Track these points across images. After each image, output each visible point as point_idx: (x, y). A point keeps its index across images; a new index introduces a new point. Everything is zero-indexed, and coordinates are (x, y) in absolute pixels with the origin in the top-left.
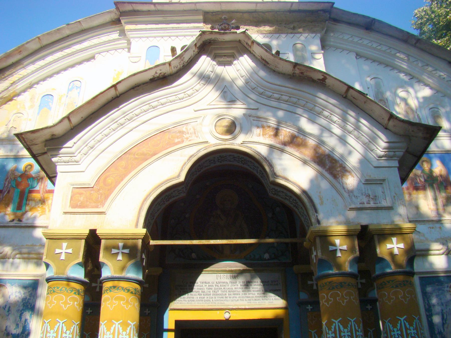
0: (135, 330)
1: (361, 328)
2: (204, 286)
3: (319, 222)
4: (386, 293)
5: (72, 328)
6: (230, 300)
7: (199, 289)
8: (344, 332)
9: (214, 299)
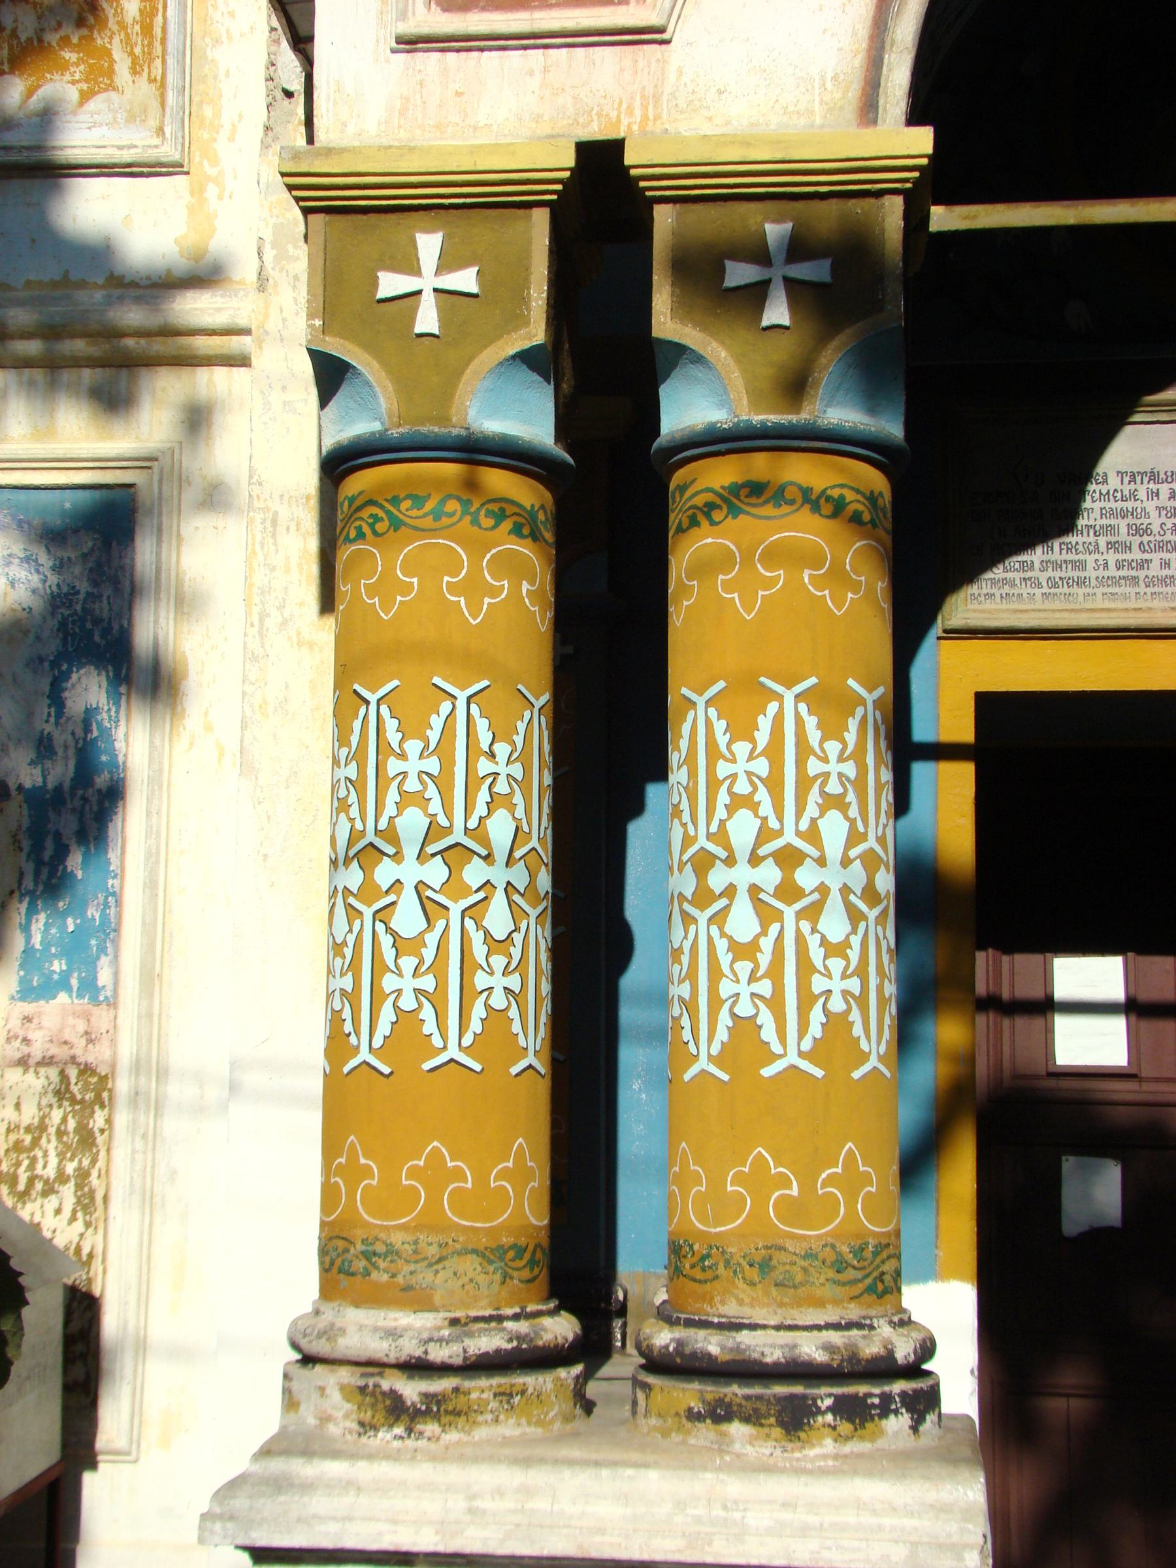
0: (882, 729)
2: (1142, 494)
5: (521, 727)
7: (1112, 513)
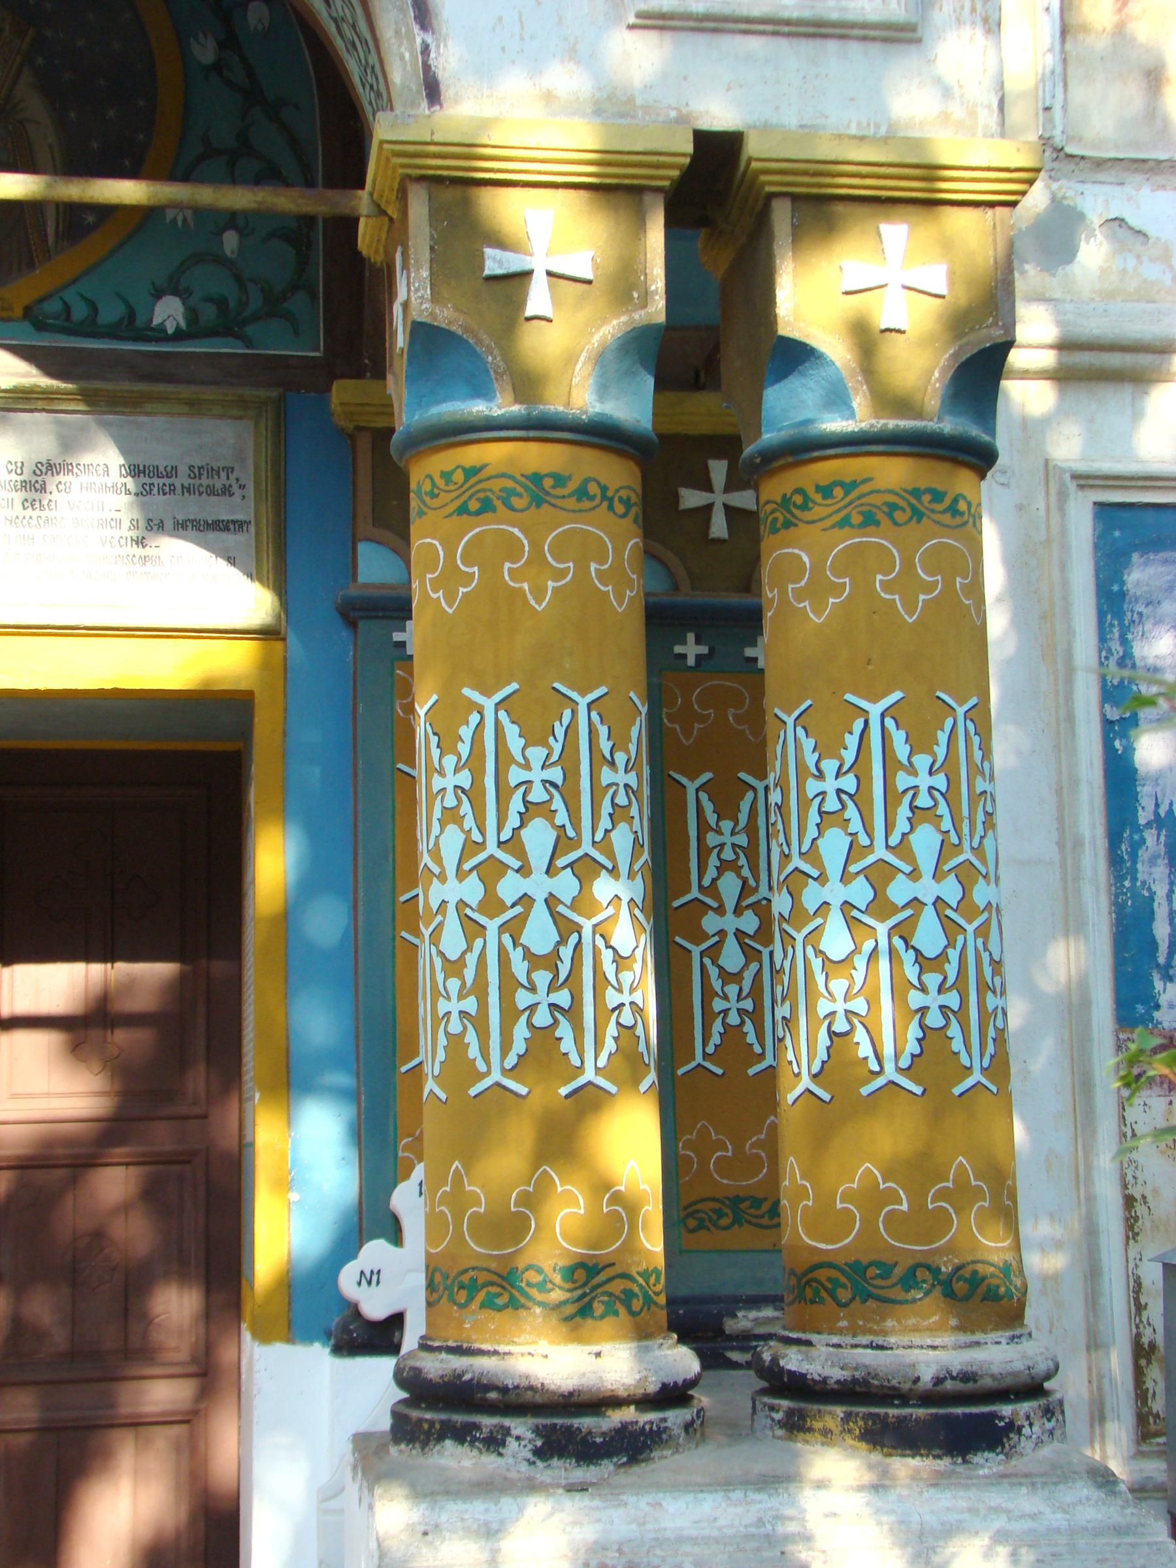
1: (633, 748)
3: (432, 90)
4: (806, 559)
8: (527, 766)
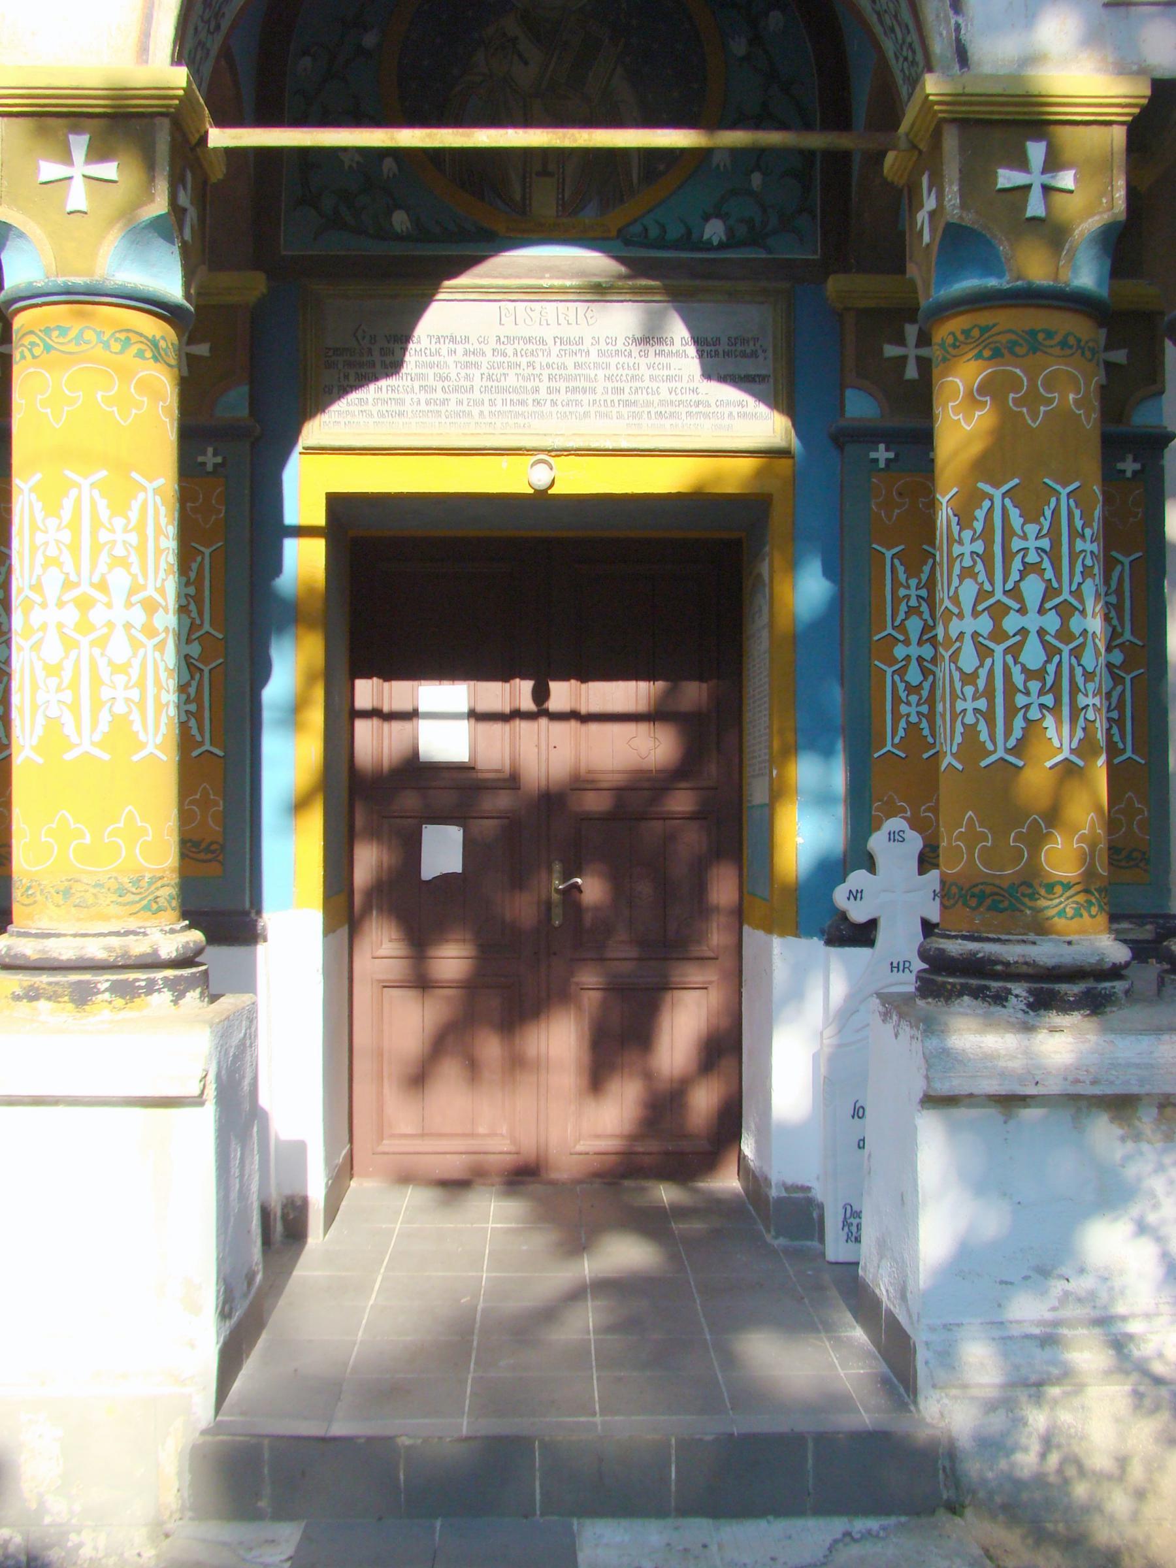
1: (1095, 525)
2: (444, 352)
6: (554, 415)
8: (1025, 537)
9: (486, 409)
